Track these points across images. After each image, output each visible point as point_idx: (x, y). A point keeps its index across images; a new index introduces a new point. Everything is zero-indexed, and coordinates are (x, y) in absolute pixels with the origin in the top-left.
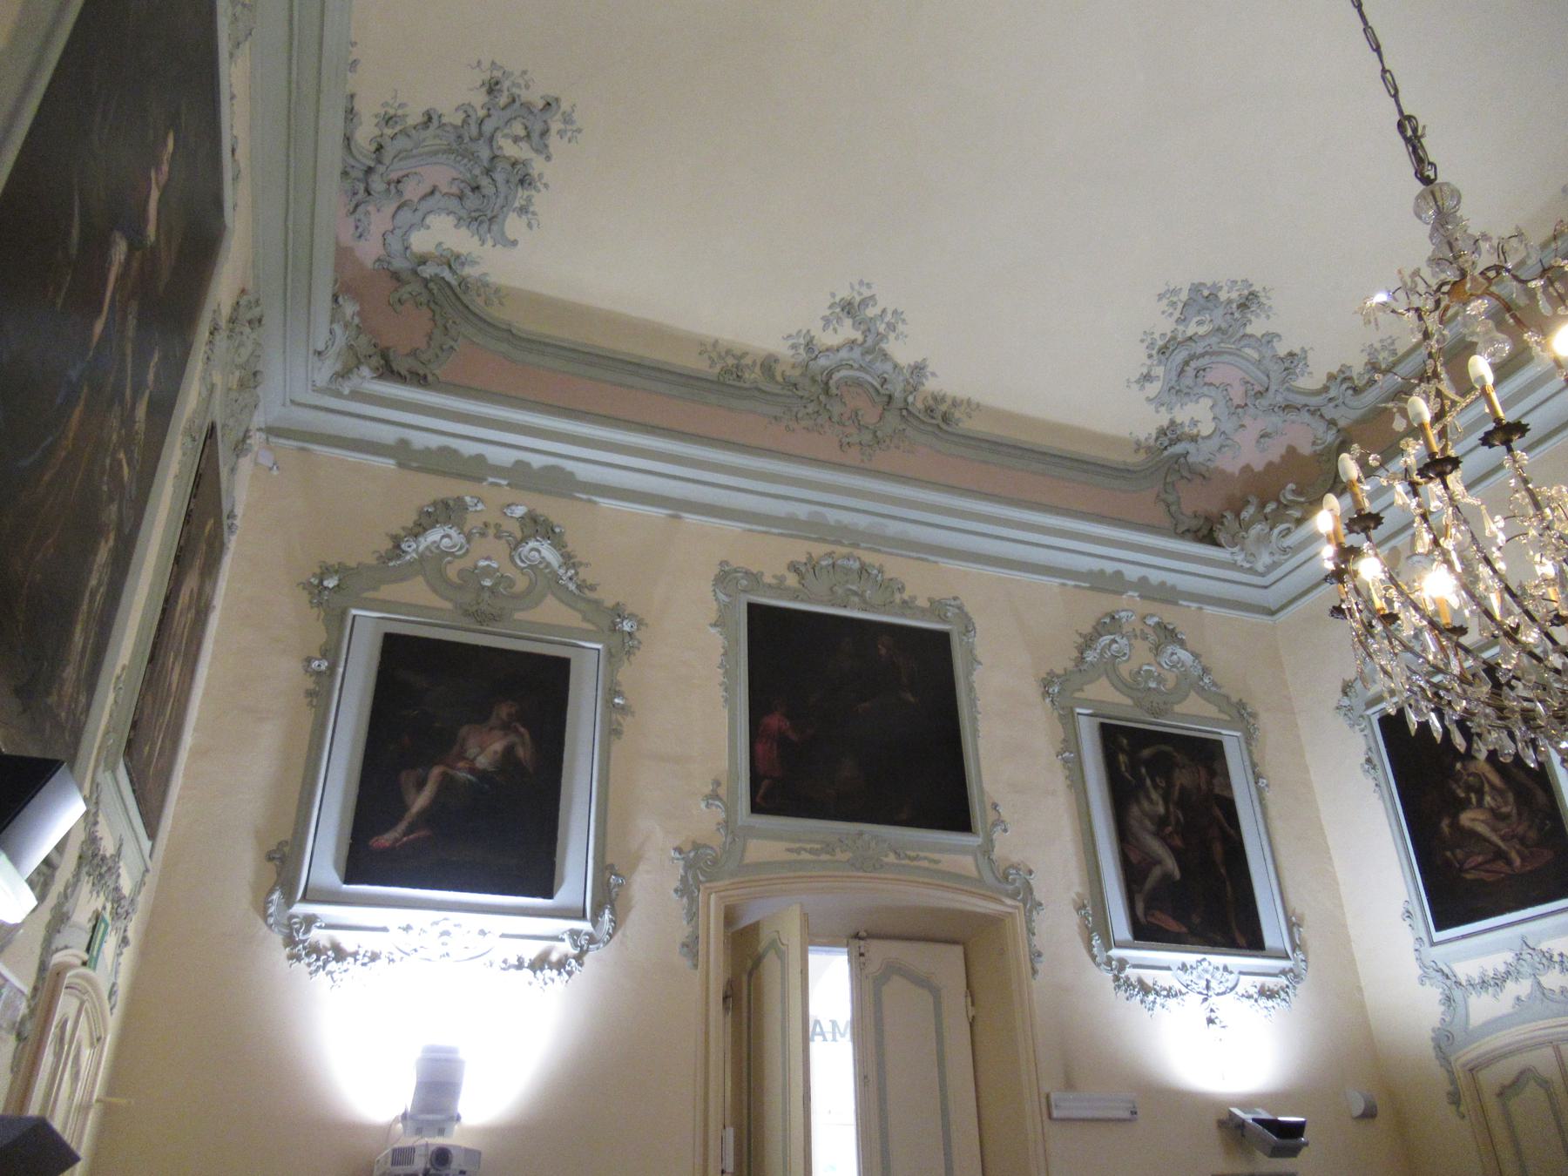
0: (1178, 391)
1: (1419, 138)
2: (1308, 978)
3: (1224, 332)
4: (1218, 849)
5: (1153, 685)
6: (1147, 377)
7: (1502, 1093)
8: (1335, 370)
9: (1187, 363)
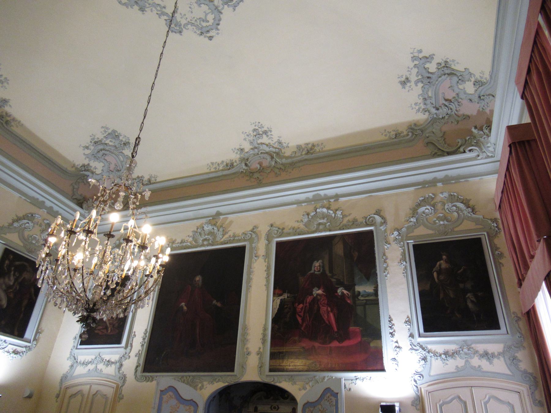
0: (95, 156)
1: (138, 145)
2: (34, 350)
3: (116, 148)
4: (25, 302)
5: (34, 242)
6: (87, 148)
7: (72, 396)
8: (140, 175)
9: (101, 150)
